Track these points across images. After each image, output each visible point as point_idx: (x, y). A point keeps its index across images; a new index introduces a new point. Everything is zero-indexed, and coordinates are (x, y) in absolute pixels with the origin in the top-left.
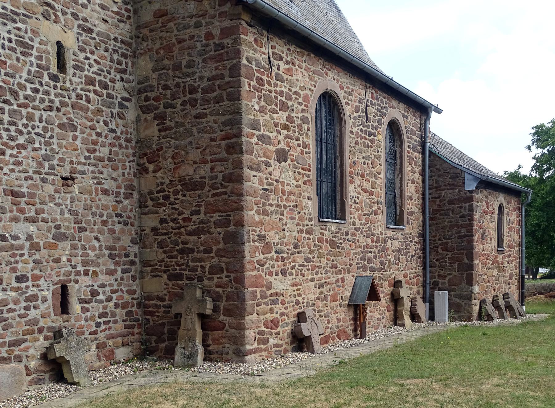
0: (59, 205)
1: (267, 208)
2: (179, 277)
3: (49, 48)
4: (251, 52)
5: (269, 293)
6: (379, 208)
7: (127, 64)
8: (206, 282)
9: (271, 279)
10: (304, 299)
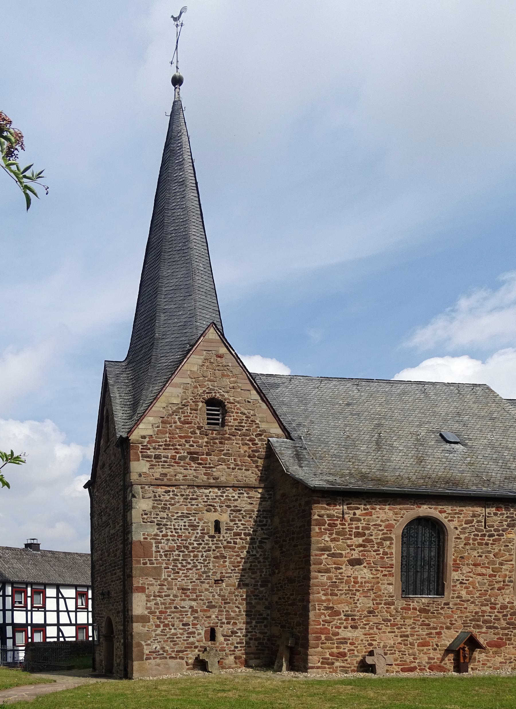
3: (210, 524)
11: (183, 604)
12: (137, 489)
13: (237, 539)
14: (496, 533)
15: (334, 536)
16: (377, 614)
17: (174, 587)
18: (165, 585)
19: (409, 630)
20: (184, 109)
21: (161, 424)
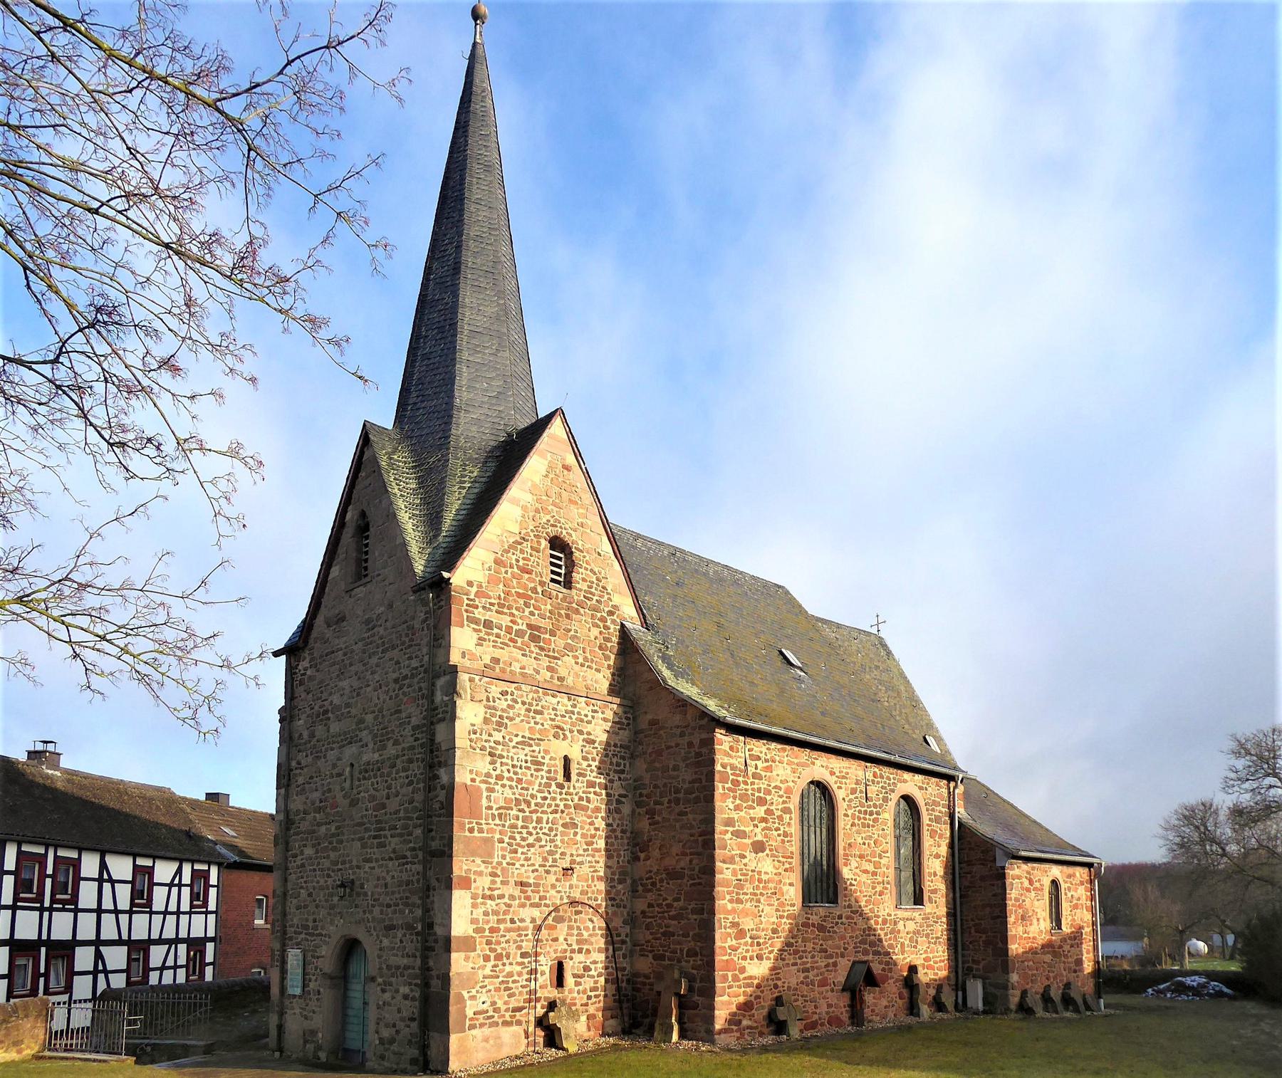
0: (559, 892)
1: (741, 897)
2: (662, 957)
4: (726, 758)
5: (742, 976)
6: (886, 889)
7: (625, 765)
8: (684, 964)
9: (744, 963)
10: (784, 983)
13: (590, 793)
15: (738, 802)
19: (809, 960)
21: (493, 565)
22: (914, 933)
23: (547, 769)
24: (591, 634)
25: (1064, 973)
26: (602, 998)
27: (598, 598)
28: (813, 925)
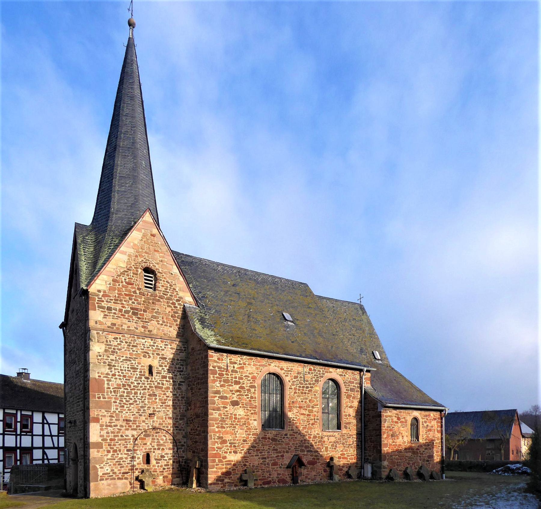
1: (224, 425)
3: (145, 368)
7: (183, 368)
11: (127, 433)
12: (93, 333)
13: (164, 381)
14: (309, 386)
15: (222, 383)
16: (248, 442)
17: (120, 418)
18: (114, 417)
19: (266, 454)
20: (135, 45)
21: (112, 282)
22: (334, 442)
23: (140, 371)
24: (167, 310)
25: (420, 462)
26: (171, 469)
27: (171, 294)
28: (269, 438)
